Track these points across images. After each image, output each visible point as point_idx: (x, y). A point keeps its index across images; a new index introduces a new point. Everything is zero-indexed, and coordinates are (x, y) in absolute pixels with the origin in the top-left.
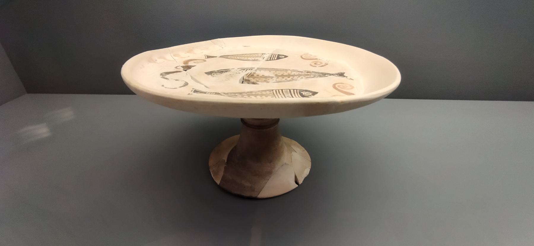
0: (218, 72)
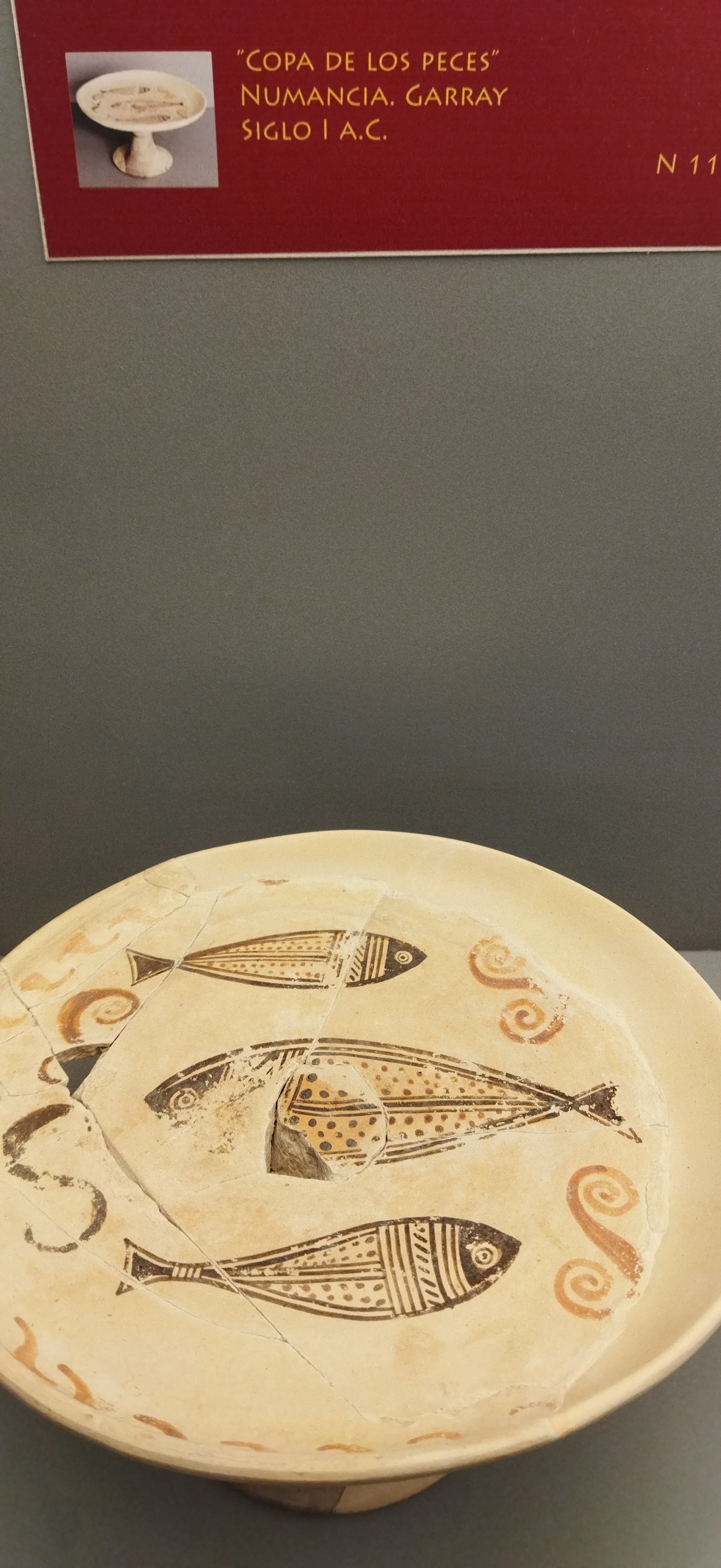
0: (189, 1083)
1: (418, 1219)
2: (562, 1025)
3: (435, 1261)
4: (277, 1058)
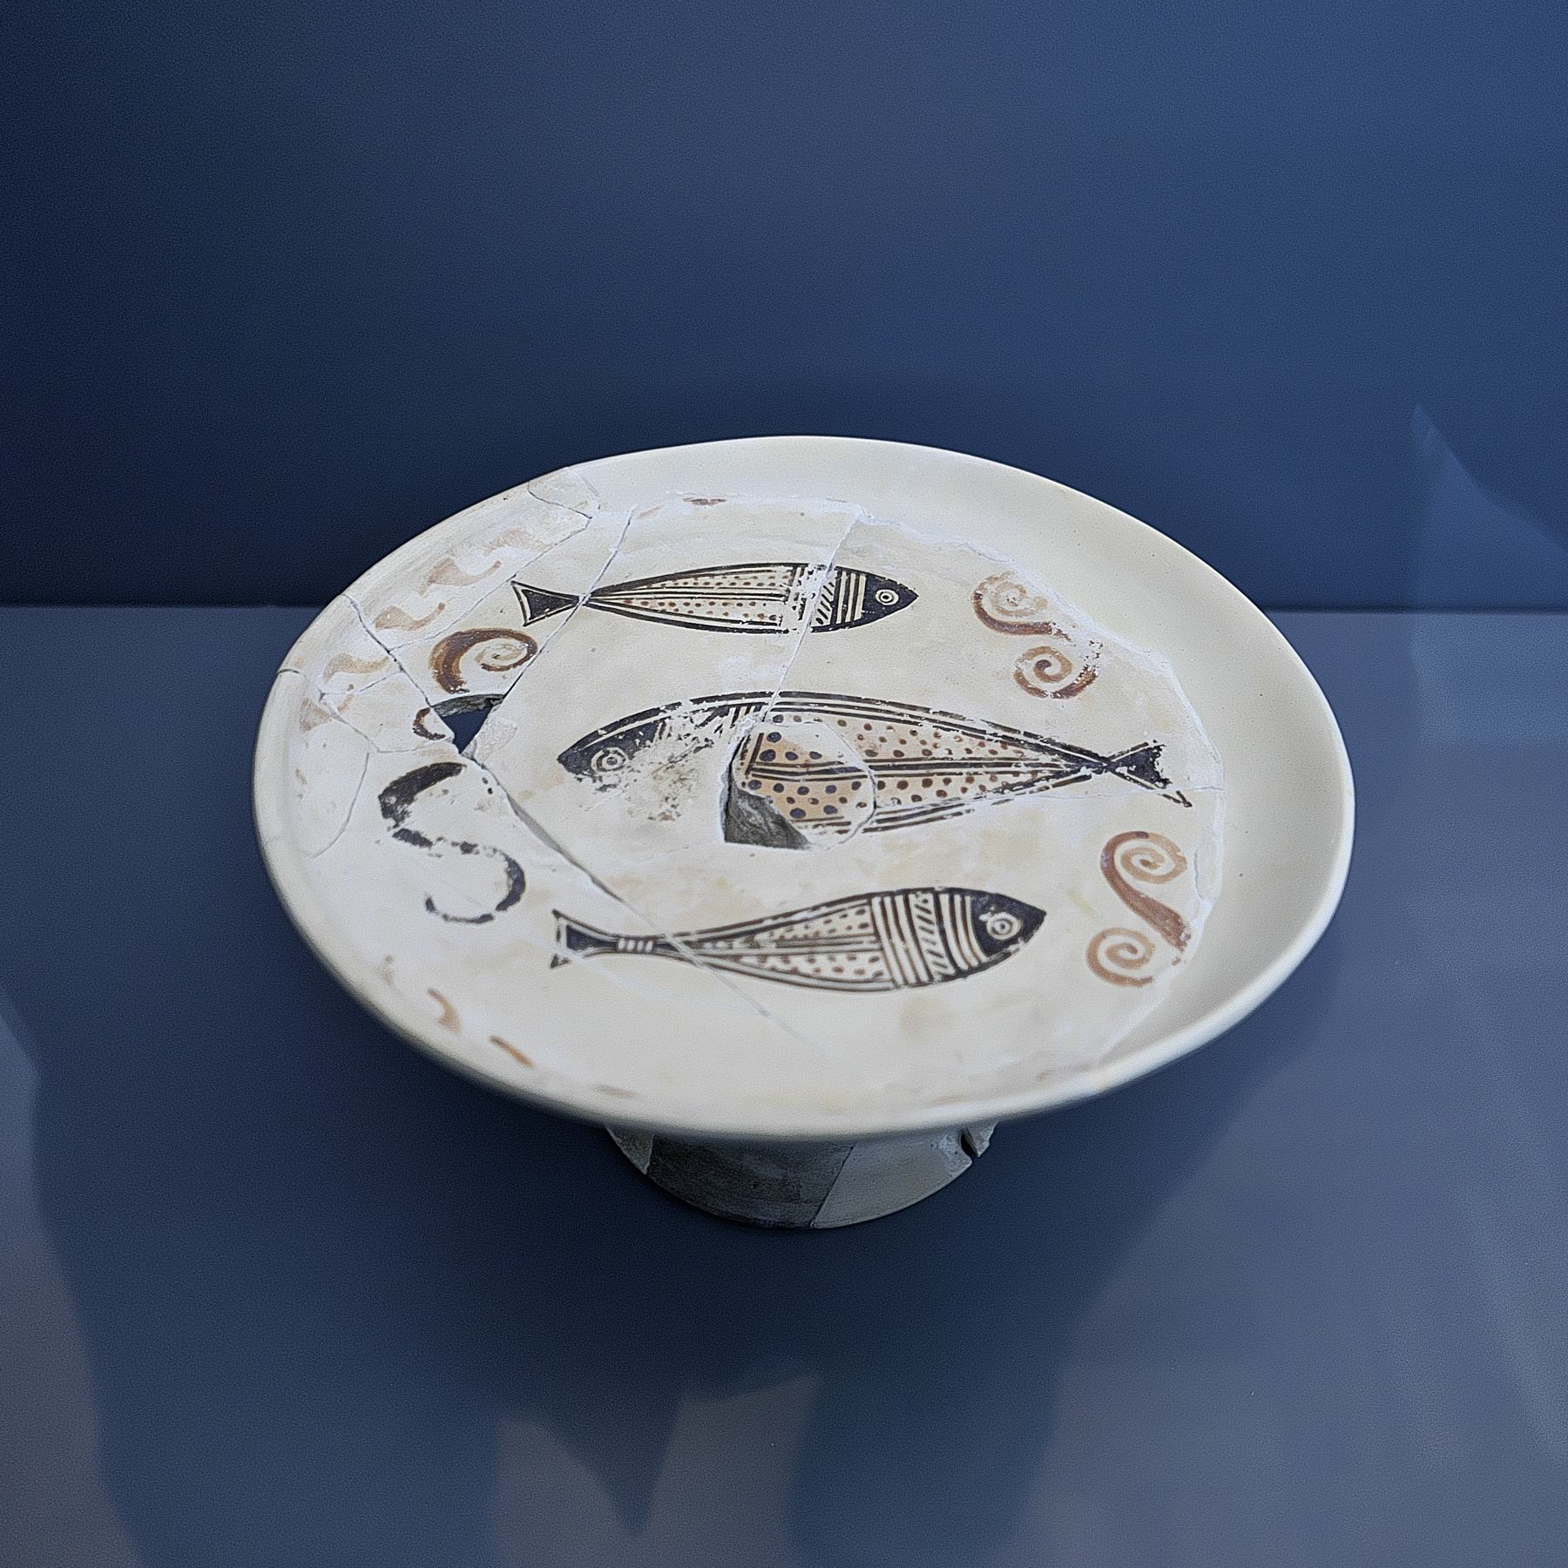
0: (613, 741)
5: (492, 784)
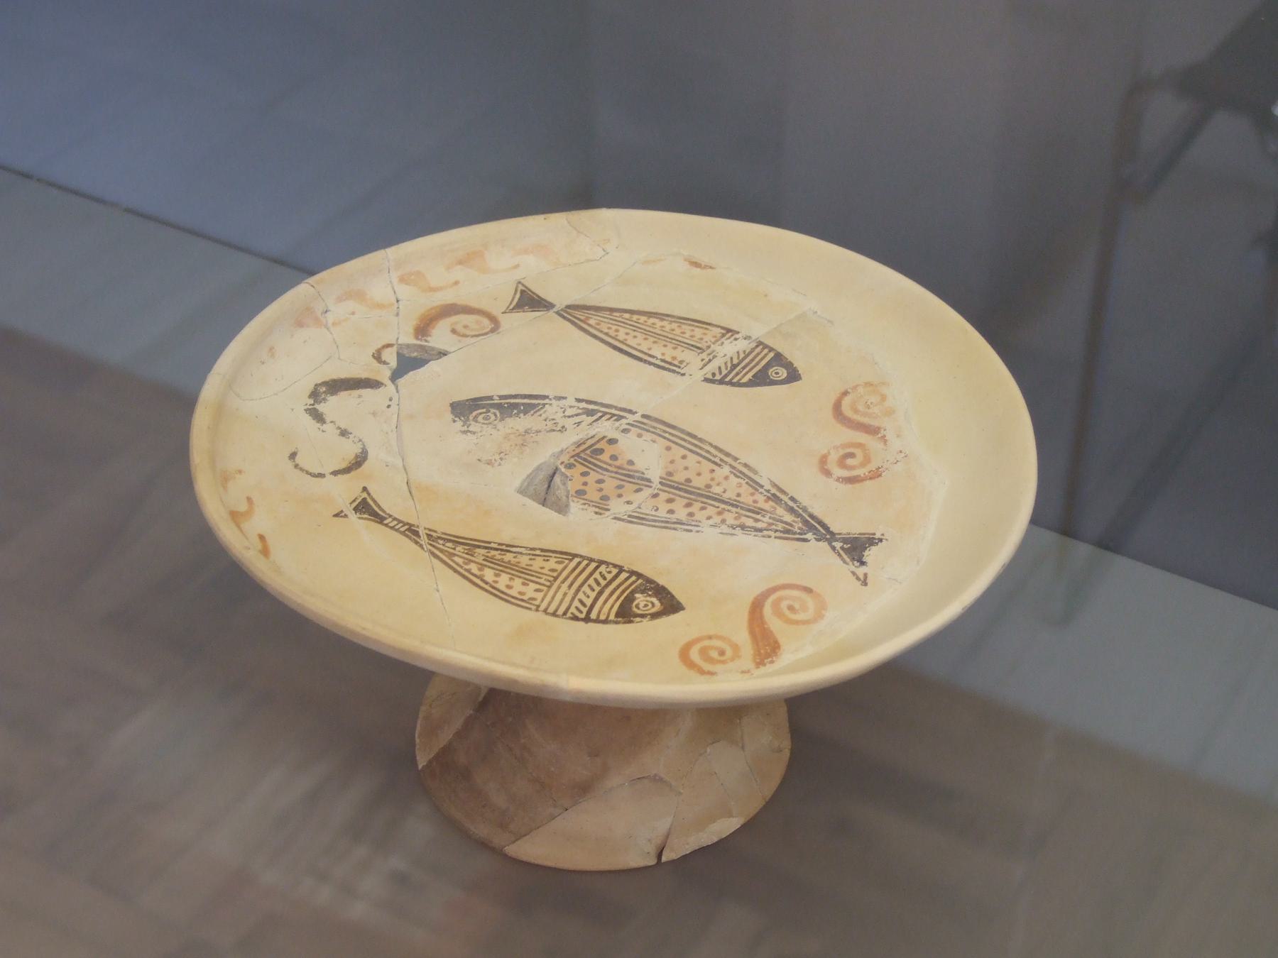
0: (499, 406)
1: (613, 564)
2: (880, 475)
3: (600, 593)
4: (592, 416)
5: (394, 403)
